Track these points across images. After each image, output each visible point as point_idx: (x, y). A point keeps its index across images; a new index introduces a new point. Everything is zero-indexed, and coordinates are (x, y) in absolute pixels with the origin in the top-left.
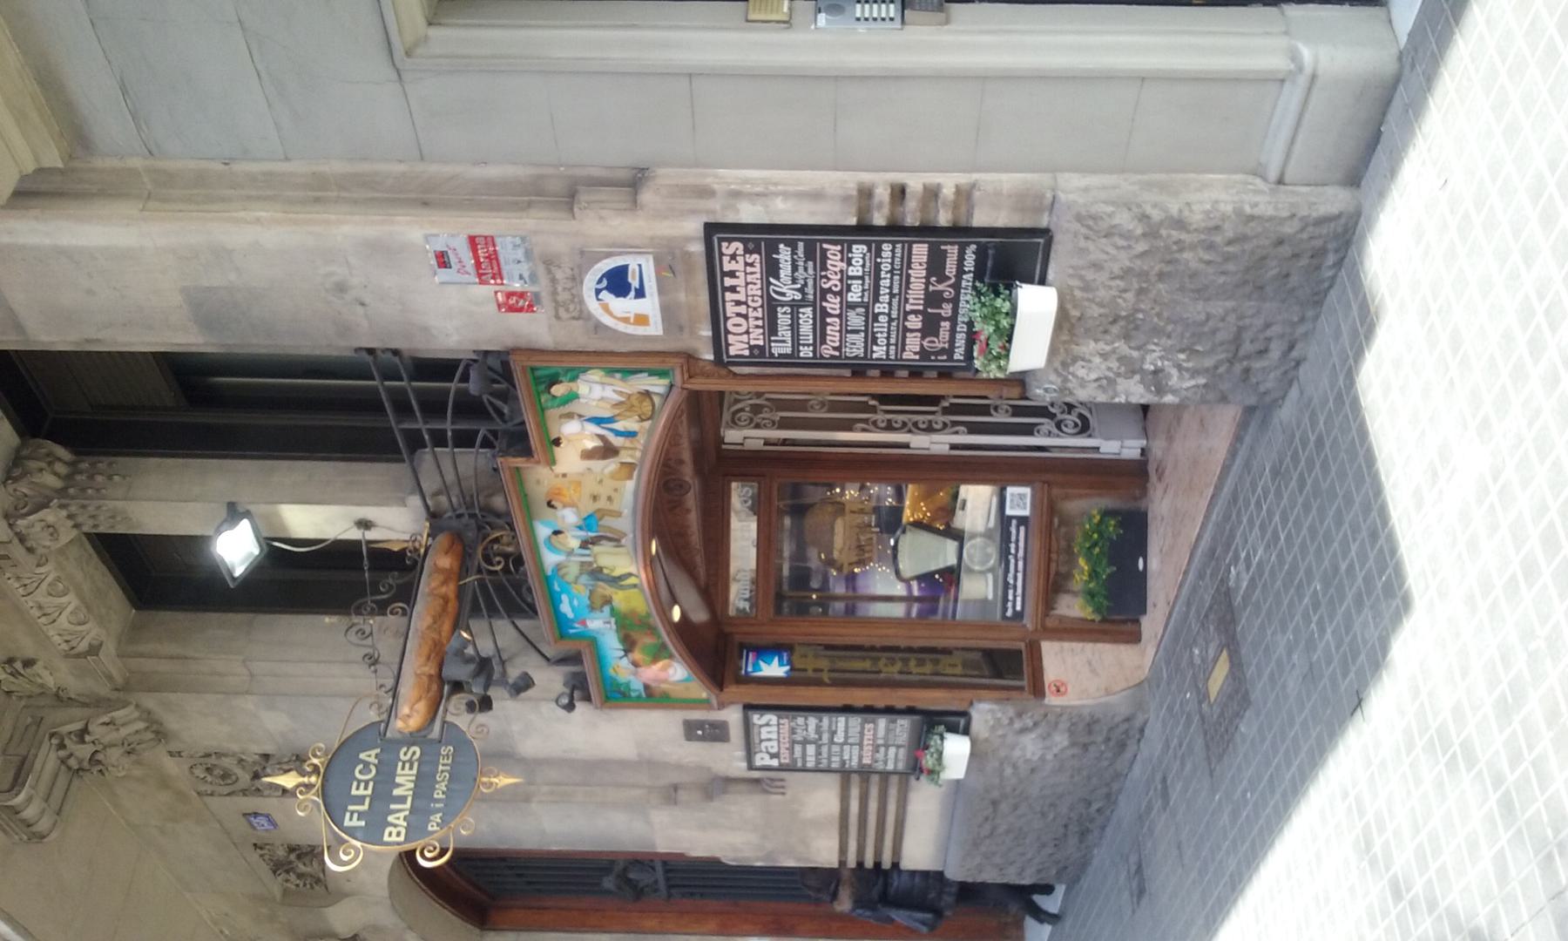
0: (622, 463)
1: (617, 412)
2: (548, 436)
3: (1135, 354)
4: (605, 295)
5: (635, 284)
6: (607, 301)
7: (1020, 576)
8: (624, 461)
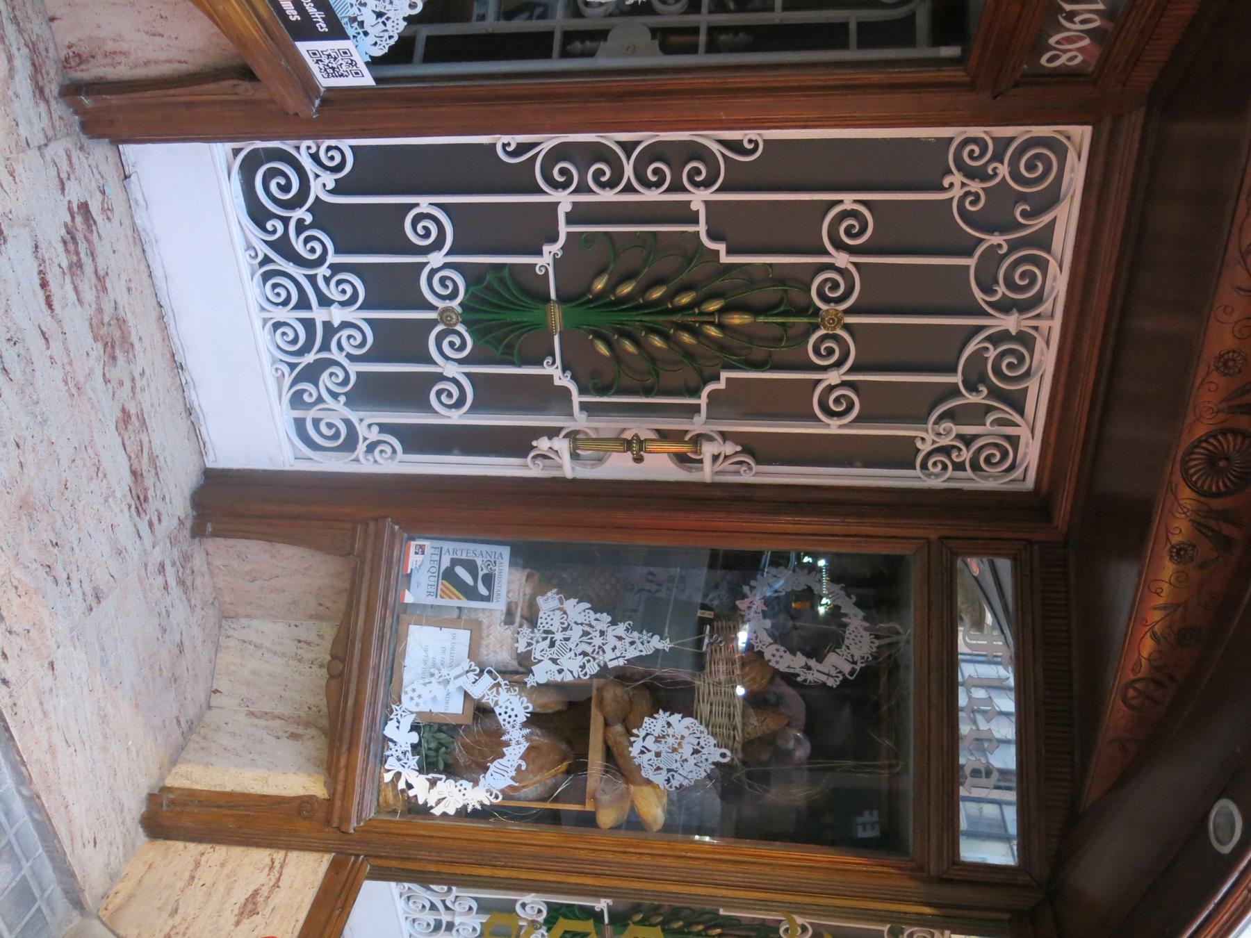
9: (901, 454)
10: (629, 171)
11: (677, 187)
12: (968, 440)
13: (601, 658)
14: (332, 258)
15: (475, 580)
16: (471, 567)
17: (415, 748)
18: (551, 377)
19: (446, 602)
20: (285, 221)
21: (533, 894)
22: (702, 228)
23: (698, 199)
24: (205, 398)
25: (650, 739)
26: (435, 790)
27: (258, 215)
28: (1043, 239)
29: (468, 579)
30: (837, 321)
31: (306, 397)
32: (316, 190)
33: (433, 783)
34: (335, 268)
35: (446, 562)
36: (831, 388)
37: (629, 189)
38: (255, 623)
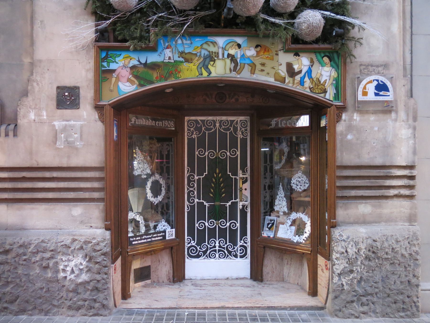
0: (285, 78)
1: (315, 79)
2: (300, 52)
3: (359, 263)
4: (376, 83)
5: (381, 93)
6: (373, 83)
7: (145, 241)
8: (286, 79)
9: (244, 141)
10: (191, 189)
11: (194, 181)
12: (241, 129)
13: (283, 197)
14: (206, 244)
15: (271, 223)
16: (268, 224)
17: (299, 236)
18: (229, 205)
19: (274, 229)
20: (200, 251)
21: (276, 201)
22: (201, 177)
23: (196, 178)
24: (235, 275)
25: (297, 187)
26: (307, 232)
27: (198, 256)
28: (203, 121)
29: (271, 224)
30: (217, 154)
31: (234, 254)
32: (194, 244)
33: (306, 232)
34: (208, 243)
35: (267, 229)
36: (226, 153)
37: (195, 189)
38: (284, 274)
